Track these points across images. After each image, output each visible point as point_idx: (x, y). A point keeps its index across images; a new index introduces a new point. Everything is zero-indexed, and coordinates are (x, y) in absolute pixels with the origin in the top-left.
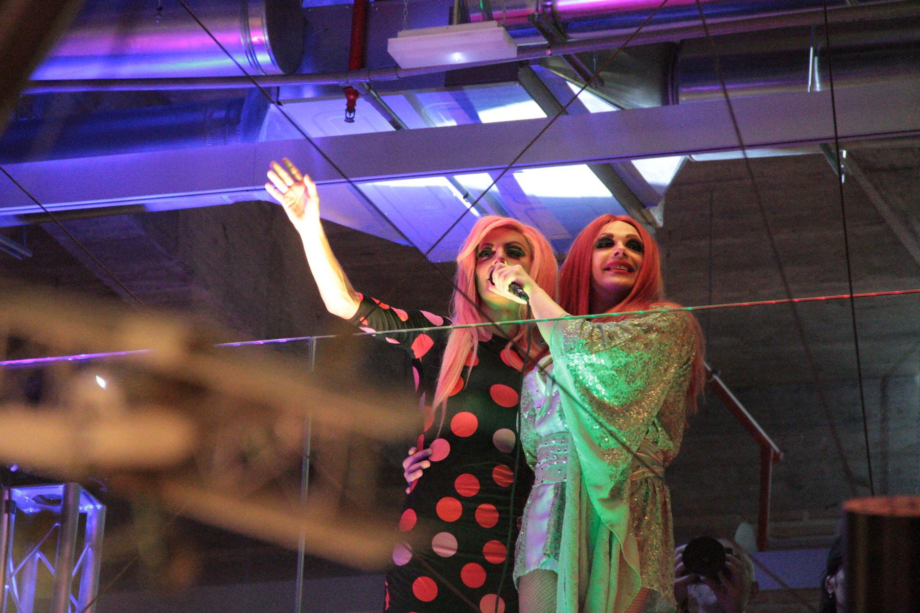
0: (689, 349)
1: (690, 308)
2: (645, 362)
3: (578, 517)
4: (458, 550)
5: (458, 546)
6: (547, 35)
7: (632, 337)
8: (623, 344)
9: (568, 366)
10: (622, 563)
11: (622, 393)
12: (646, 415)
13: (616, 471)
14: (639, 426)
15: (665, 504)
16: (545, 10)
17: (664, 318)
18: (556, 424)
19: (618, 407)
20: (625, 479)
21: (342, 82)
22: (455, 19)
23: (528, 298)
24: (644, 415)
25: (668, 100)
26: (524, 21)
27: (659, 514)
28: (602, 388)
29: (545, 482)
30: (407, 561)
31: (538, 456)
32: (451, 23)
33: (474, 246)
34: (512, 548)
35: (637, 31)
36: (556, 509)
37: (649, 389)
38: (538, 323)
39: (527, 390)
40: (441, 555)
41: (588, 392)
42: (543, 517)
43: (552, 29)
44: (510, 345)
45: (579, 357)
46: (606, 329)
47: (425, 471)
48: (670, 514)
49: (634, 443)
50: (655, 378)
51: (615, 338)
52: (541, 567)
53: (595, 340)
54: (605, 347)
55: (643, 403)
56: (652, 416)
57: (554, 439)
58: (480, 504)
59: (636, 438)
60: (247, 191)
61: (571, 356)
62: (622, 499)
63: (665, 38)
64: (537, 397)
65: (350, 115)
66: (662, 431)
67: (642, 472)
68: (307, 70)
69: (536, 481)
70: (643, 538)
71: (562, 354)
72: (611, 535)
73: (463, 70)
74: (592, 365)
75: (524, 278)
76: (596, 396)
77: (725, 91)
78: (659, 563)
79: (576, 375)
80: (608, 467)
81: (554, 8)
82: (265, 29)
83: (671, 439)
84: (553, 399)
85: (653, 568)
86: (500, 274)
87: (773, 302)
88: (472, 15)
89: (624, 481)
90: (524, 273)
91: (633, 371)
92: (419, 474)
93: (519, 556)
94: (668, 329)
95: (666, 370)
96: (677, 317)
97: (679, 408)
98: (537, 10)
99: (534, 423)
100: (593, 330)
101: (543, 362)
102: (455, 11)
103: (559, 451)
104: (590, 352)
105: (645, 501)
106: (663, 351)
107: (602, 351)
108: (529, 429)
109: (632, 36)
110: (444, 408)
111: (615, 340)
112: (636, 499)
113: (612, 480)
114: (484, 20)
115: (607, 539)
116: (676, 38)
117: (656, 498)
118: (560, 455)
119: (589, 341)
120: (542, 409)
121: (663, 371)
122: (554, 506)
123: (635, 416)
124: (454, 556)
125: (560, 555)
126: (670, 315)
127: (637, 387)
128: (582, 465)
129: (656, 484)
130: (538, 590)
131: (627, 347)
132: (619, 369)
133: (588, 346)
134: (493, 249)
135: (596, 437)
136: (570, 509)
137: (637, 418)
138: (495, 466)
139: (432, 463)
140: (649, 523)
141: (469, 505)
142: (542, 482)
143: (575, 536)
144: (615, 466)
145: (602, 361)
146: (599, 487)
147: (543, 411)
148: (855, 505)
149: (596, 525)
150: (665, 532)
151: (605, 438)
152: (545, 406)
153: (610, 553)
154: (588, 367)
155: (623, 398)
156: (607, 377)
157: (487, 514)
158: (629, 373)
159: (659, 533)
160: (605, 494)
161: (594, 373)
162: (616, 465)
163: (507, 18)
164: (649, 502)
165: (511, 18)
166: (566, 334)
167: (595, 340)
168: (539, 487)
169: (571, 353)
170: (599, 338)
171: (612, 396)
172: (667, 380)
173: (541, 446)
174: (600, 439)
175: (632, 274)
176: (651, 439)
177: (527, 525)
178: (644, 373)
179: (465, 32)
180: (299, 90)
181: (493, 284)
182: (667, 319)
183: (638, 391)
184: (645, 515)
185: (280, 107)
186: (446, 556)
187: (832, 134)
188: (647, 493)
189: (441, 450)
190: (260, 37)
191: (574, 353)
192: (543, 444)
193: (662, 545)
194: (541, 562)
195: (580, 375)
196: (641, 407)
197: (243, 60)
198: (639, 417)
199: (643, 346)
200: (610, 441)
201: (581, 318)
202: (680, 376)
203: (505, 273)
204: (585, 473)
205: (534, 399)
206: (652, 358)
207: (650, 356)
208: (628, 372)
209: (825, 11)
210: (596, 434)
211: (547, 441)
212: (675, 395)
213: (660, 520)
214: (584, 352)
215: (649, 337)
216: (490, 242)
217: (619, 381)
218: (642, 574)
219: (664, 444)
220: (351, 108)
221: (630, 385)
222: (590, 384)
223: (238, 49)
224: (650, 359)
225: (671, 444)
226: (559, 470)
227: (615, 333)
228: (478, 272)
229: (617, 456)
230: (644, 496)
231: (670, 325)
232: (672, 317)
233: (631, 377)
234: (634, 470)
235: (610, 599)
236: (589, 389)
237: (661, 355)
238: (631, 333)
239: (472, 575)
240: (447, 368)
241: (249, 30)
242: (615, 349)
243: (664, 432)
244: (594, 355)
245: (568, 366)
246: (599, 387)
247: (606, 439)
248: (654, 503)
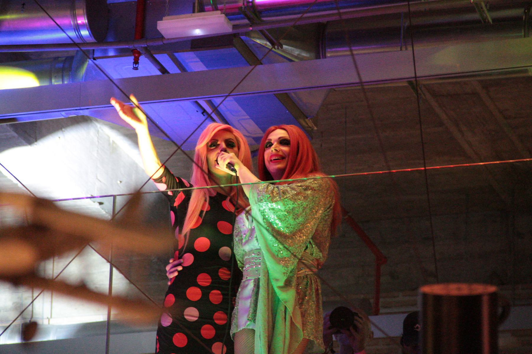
0: (331, 200)
1: (333, 176)
2: (304, 207)
3: (267, 297)
4: (199, 318)
5: (199, 315)
6: (249, 19)
7: (297, 193)
8: (291, 197)
9: (259, 210)
10: (292, 324)
11: (291, 225)
12: (304, 238)
13: (287, 270)
14: (300, 244)
15: (317, 290)
16: (248, 4)
17: (316, 182)
18: (254, 245)
19: (288, 233)
20: (293, 275)
21: (131, 46)
22: (196, 10)
23: (236, 172)
24: (303, 238)
25: (320, 56)
26: (237, 11)
27: (314, 296)
28: (279, 222)
29: (248, 278)
30: (169, 324)
31: (245, 263)
32: (194, 12)
33: (208, 140)
34: (231, 316)
35: (301, 16)
36: (255, 293)
37: (306, 223)
38: (242, 186)
39: (238, 225)
40: (189, 321)
41: (271, 225)
42: (247, 298)
43: (252, 15)
44: (229, 198)
45: (266, 205)
46: (281, 188)
47: (179, 272)
48: (320, 296)
50: (310, 217)
51: (287, 193)
52: (247, 327)
53: (275, 195)
54: (280, 199)
55: (303, 231)
56: (308, 238)
57: (254, 253)
58: (212, 290)
59: (298, 251)
60: (76, 110)
61: (261, 204)
62: (291, 287)
63: (315, 21)
64: (243, 229)
65: (136, 65)
66: (315, 247)
67: (305, 271)
68: (110, 39)
69: (243, 278)
70: (304, 310)
71: (256, 203)
72: (286, 308)
73: (200, 39)
74: (273, 209)
75: (235, 160)
76: (275, 227)
77: (351, 51)
78: (314, 324)
79: (264, 215)
80: (282, 268)
81: (253, 3)
82: (86, 16)
83: (321, 251)
84: (253, 230)
85: (310, 326)
86: (222, 158)
87: (381, 172)
88: (206, 7)
89: (293, 276)
90: (235, 157)
91: (297, 212)
92: (176, 274)
93: (234, 321)
94: (318, 188)
95: (316, 212)
96: (323, 181)
97: (325, 234)
98: (244, 4)
99: (242, 244)
100: (273, 189)
101: (248, 209)
102: (196, 5)
103: (256, 260)
104: (272, 202)
105: (306, 288)
106: (314, 201)
107: (279, 201)
108: (239, 247)
109: (300, 18)
110: (188, 235)
111: (286, 195)
112: (301, 287)
113: (285, 276)
114: (213, 10)
115: (283, 310)
116: (324, 20)
117: (312, 286)
118: (257, 262)
119: (271, 195)
120: (246, 236)
121: (315, 212)
122: (254, 292)
123: (298, 238)
124: (196, 321)
125: (256, 321)
126: (319, 180)
127: (300, 222)
128: (268, 267)
129: (312, 278)
130: (243, 339)
131: (294, 199)
132: (289, 211)
133: (271, 198)
134: (219, 143)
135: (276, 251)
136: (262, 293)
137: (299, 240)
138: (219, 268)
139: (183, 267)
140: (308, 301)
141: (206, 291)
142: (247, 278)
143: (266, 308)
144: (286, 268)
145: (279, 207)
146: (277, 280)
147: (247, 237)
148: (426, 289)
149: (277, 302)
150: (318, 306)
151: (280, 251)
152: (248, 234)
153: (285, 318)
154: (271, 211)
155: (291, 228)
156: (282, 216)
157: (216, 296)
158: (295, 214)
159: (314, 307)
160: (281, 284)
161: (274, 214)
162: (287, 267)
163: (226, 9)
164: (308, 289)
165: (230, 9)
166: (258, 192)
167: (275, 195)
168: (245, 281)
169: (261, 203)
170: (277, 194)
171: (285, 227)
172: (317, 217)
173: (246, 257)
174: (278, 252)
176: (309, 252)
177: (238, 303)
178: (304, 214)
179: (202, 17)
180: (106, 51)
181: (218, 164)
182: (317, 183)
183: (300, 224)
184: (306, 296)
185: (95, 61)
186: (192, 321)
187: (413, 75)
188: (307, 284)
189: (189, 259)
190: (83, 20)
191: (263, 202)
192: (247, 256)
193: (316, 313)
194: (247, 324)
195: (266, 215)
196: (303, 233)
197: (72, 34)
198: (301, 239)
199: (303, 198)
200: (284, 253)
201: (267, 183)
202: (326, 216)
203: (224, 158)
204: (269, 272)
205: (242, 230)
206: (309, 205)
207: (307, 203)
208: (294, 213)
209: (409, 5)
210: (276, 249)
211: (250, 254)
212: (323, 227)
213: (315, 299)
214: (268, 202)
215: (306, 193)
216: (216, 138)
217: (289, 218)
218: (303, 331)
219: (317, 255)
220: (136, 62)
221: (295, 220)
222: (272, 220)
223: (70, 27)
224: (307, 205)
225: (321, 254)
226: (257, 271)
227: (287, 190)
228: (209, 155)
229: (287, 261)
230: (305, 286)
231: (319, 186)
232: (320, 181)
233: (296, 216)
234: (299, 270)
236: (272, 223)
237: (314, 203)
238: (296, 191)
239: (207, 332)
240: (191, 213)
241: (76, 17)
242: (286, 200)
243: (316, 248)
244: (274, 203)
245: (260, 210)
246: (278, 222)
247: (281, 252)
248: (311, 289)
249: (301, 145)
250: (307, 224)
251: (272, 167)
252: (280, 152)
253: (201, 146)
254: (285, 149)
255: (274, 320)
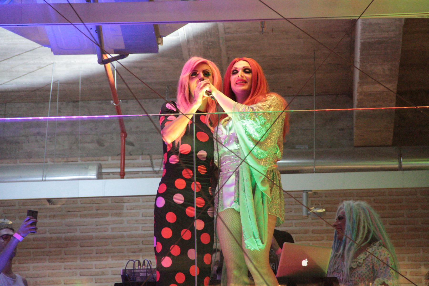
9: (242, 125)
17: (274, 101)
49: (271, 156)
55: (272, 138)
60: (18, 25)
71: (239, 120)
115: (260, 196)
118: (237, 159)
141: (189, 182)
142: (229, 171)
151: (259, 155)
154: (251, 125)
174: (257, 156)
175: (247, 84)
191: (245, 119)
216: (196, 70)
228: (191, 82)
235: (261, 218)
247: (260, 156)
249: (259, 74)
250: (273, 133)
251: (237, 89)
252: (245, 77)
253: (184, 75)
254: (249, 76)
255: (106, 174)
